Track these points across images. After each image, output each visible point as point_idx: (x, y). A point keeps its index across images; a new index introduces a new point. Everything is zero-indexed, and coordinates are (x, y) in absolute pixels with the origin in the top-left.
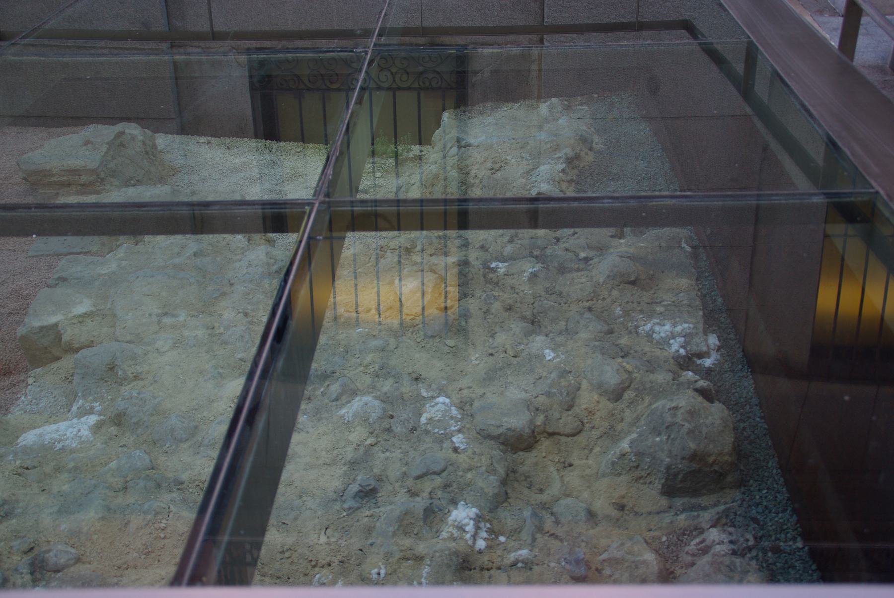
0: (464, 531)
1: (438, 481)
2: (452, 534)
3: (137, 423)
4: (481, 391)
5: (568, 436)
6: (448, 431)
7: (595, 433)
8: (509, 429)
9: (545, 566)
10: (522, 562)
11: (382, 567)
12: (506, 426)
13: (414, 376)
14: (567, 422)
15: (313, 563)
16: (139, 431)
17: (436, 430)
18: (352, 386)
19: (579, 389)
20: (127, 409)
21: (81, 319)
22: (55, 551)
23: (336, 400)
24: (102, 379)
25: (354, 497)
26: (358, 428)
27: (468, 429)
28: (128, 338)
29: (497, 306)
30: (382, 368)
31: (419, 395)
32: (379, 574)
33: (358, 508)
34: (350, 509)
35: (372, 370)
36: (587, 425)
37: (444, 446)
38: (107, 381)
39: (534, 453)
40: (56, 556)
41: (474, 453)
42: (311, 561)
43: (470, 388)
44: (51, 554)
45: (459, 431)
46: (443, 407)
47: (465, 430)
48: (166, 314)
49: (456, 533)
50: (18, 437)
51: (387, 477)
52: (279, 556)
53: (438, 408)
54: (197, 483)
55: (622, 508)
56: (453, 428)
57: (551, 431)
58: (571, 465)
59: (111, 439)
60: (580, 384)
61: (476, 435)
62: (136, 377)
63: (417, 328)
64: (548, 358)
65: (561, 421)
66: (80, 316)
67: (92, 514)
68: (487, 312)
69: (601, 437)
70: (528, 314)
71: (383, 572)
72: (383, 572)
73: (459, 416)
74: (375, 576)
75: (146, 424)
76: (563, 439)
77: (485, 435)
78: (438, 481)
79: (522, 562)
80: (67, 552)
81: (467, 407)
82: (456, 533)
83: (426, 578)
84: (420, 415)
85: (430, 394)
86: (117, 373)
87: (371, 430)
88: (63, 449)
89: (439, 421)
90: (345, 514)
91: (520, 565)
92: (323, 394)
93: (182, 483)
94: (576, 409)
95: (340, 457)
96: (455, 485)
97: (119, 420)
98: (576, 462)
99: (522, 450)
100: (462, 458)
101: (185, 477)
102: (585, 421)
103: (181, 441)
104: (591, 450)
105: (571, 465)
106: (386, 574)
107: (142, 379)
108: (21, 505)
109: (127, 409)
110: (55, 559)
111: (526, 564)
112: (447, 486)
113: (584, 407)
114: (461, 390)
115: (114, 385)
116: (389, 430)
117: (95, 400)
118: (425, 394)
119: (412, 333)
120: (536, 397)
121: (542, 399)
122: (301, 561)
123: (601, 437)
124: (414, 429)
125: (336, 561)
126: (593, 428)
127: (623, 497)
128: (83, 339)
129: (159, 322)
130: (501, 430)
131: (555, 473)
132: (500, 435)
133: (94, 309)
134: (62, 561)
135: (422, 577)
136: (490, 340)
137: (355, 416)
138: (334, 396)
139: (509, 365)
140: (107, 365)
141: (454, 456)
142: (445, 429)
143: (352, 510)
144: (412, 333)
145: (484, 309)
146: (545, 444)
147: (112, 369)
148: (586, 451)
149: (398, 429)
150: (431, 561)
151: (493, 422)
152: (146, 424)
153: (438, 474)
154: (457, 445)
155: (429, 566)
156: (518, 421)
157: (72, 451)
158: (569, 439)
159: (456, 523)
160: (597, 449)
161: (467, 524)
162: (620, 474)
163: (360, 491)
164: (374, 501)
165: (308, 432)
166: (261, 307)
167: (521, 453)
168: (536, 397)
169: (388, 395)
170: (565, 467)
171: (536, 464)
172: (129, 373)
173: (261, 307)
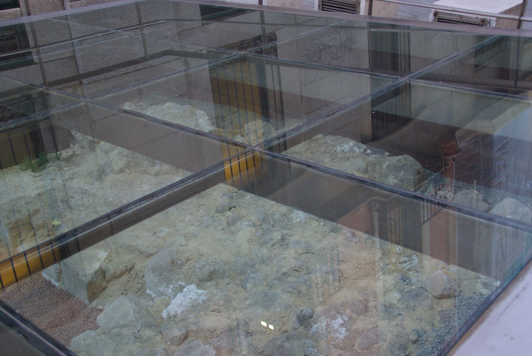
3: (223, 272)
16: (227, 275)
20: (214, 268)
93: (286, 273)
97: (212, 276)
101: (285, 270)
109: (214, 268)
117: (177, 282)
157: (209, 300)
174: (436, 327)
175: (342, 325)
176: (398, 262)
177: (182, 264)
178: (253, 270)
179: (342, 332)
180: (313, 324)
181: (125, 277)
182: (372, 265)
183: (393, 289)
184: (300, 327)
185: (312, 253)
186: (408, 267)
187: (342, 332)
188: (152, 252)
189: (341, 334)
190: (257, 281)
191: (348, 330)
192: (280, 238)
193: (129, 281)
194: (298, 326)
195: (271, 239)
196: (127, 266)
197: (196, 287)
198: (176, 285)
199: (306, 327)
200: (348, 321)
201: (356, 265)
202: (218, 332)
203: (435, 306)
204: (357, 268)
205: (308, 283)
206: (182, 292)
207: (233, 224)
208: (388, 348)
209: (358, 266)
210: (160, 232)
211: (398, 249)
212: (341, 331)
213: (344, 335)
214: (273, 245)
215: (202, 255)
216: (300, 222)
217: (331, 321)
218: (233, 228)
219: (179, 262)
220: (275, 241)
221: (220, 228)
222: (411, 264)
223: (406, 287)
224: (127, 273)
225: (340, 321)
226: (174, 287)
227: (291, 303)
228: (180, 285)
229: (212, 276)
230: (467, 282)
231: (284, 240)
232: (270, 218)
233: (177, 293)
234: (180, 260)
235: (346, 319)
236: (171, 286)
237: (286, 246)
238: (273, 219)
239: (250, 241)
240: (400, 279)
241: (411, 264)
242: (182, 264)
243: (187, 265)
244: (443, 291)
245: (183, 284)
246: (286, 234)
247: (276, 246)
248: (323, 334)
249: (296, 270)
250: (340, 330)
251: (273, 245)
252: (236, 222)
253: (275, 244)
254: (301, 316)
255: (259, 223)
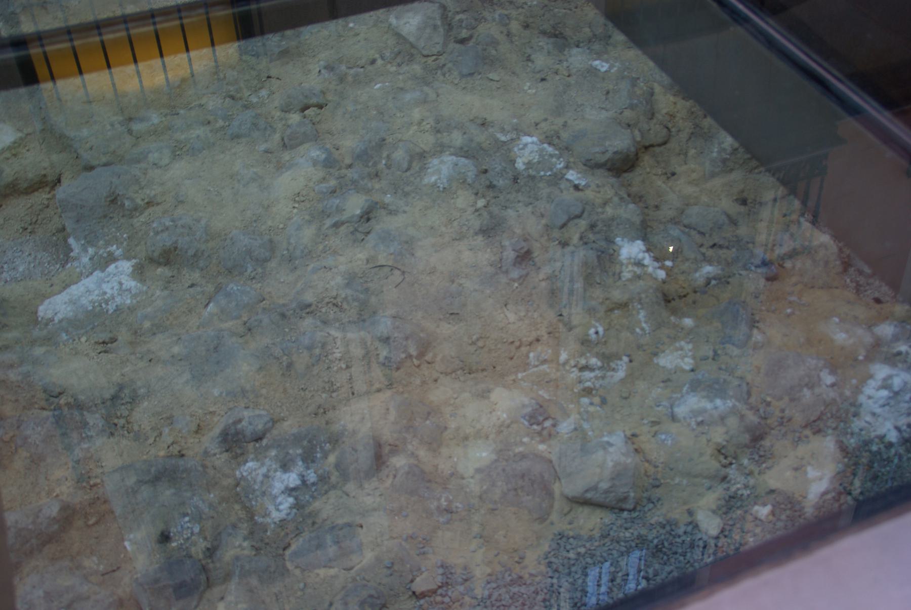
0: (643, 265)
1: (583, 223)
2: (635, 272)
3: (195, 255)
4: (560, 121)
5: (660, 145)
6: (555, 170)
7: (684, 136)
8: (615, 153)
9: (737, 276)
10: (715, 278)
11: (597, 324)
12: (611, 150)
13: (479, 121)
14: (656, 133)
15: (517, 344)
16: (202, 264)
17: (542, 173)
18: (418, 150)
19: (652, 94)
20: (176, 242)
21: (14, 152)
22: (247, 419)
23: (408, 169)
24: (105, 216)
25: (514, 265)
26: (460, 192)
27: (574, 163)
28: (104, 160)
29: (515, 26)
30: (438, 122)
31: (497, 140)
32: (597, 333)
33: (527, 275)
34: (521, 277)
35: (429, 126)
36: (673, 130)
37: (562, 186)
38: (111, 218)
39: (638, 171)
40: (250, 424)
41: (598, 186)
42: (512, 343)
43: (546, 120)
44: (243, 423)
45: (567, 167)
46: (536, 148)
47: (572, 165)
48: (130, 119)
49: (638, 270)
50: (36, 313)
51: (529, 235)
52: (472, 349)
53: (529, 149)
54: (327, 300)
55: (744, 202)
56: (559, 166)
57: (647, 144)
58: (673, 174)
59: (169, 282)
60: (652, 89)
61: (585, 168)
62: (149, 204)
63: (445, 69)
64: (603, 69)
65: (651, 132)
66: (9, 148)
67: (245, 367)
68: (509, 34)
69: (690, 138)
70: (547, 27)
71: (601, 330)
72: (601, 330)
73: (557, 152)
74: (594, 336)
75: (206, 254)
76: (657, 150)
77: (592, 166)
78: (583, 223)
79: (715, 278)
80: (259, 416)
81: (556, 141)
82: (638, 270)
83: (646, 322)
84: (513, 162)
85: (509, 137)
86: (123, 205)
87: (475, 191)
88: (118, 309)
89: (539, 162)
90: (516, 285)
91: (713, 282)
92: (388, 167)
93: (310, 305)
94: (659, 116)
95: (465, 228)
96: (599, 223)
97: (168, 257)
98: (678, 170)
99: (625, 171)
100: (589, 194)
101: (309, 297)
102: (670, 125)
103: (266, 260)
104: (686, 154)
105: (673, 174)
106: (605, 330)
107: (158, 204)
108: (139, 383)
109: (176, 242)
110: (251, 427)
111: (720, 279)
112: (592, 226)
113: (664, 111)
114: (537, 124)
115: (122, 220)
116: (491, 186)
117: (108, 243)
118: (503, 138)
119: (444, 75)
120: (621, 113)
121: (628, 113)
122: (499, 346)
123: (690, 138)
124: (515, 180)
125: (543, 332)
126: (679, 131)
127: (743, 191)
128: (30, 175)
129: (130, 132)
130: (608, 155)
131: (663, 186)
132: (607, 161)
133: (20, 135)
134: (260, 427)
135: (640, 322)
136: (530, 64)
137: (450, 180)
138: (405, 165)
139: (568, 86)
140: (107, 197)
141: (580, 194)
142: (551, 169)
143: (523, 278)
144: (444, 75)
145: (505, 32)
146: (647, 160)
147: (113, 201)
148: (682, 156)
149: (501, 183)
150: (641, 304)
151: (597, 149)
152: (206, 254)
153: (579, 217)
154: (577, 182)
155: (642, 309)
156: (621, 142)
157: (132, 309)
158: (662, 148)
159: (632, 261)
160: (692, 152)
161: (644, 258)
162: (731, 170)
163: (518, 256)
164: (531, 262)
165: (405, 212)
166: (242, 85)
167: (625, 175)
168: (621, 113)
169: (466, 149)
170: (668, 178)
171: (643, 182)
172: (139, 201)
173: (242, 85)
174: (525, 567)
175: (290, 491)
176: (572, 363)
177: (136, 209)
178: (260, 270)
179: (281, 507)
180: (252, 456)
181: (41, 197)
182: (513, 348)
183: (492, 436)
184: (221, 453)
185: (403, 273)
186: (588, 384)
187: (281, 507)
188: (94, 163)
189: (278, 510)
190: (234, 304)
191: (298, 506)
192: (358, 212)
193: (47, 207)
194: (216, 451)
195: (340, 210)
196: (45, 176)
197: (131, 269)
198: (101, 252)
199: (236, 457)
200: (313, 484)
201: (474, 337)
202: (62, 401)
203: (554, 517)
204: (474, 343)
205: (317, 351)
206: (103, 271)
207: (293, 147)
208: (344, 588)
209: (478, 340)
210: (142, 120)
211: (592, 331)
212: (280, 504)
213: (282, 515)
214: (336, 225)
215: (182, 202)
216: (434, 185)
217: (276, 471)
218: (286, 156)
219: (127, 203)
220: (345, 216)
221: (263, 147)
222: (603, 378)
223: (526, 440)
224: (48, 189)
225: (292, 479)
226: (96, 253)
227: (248, 387)
228: (110, 254)
229: (168, 257)
230: (685, 482)
231: (368, 220)
232: (385, 155)
233: (95, 270)
234: (132, 200)
235: (312, 477)
236: (91, 251)
237: (360, 236)
238: (388, 157)
239: (298, 198)
240: (524, 417)
241: (603, 378)
242: (136, 209)
243: (146, 213)
244: (587, 491)
245: (118, 252)
246: (384, 207)
247: (343, 229)
248: (254, 491)
249: (335, 305)
250: (280, 499)
251: (336, 225)
252: (301, 143)
253: (343, 223)
254: (232, 431)
255: (348, 161)
